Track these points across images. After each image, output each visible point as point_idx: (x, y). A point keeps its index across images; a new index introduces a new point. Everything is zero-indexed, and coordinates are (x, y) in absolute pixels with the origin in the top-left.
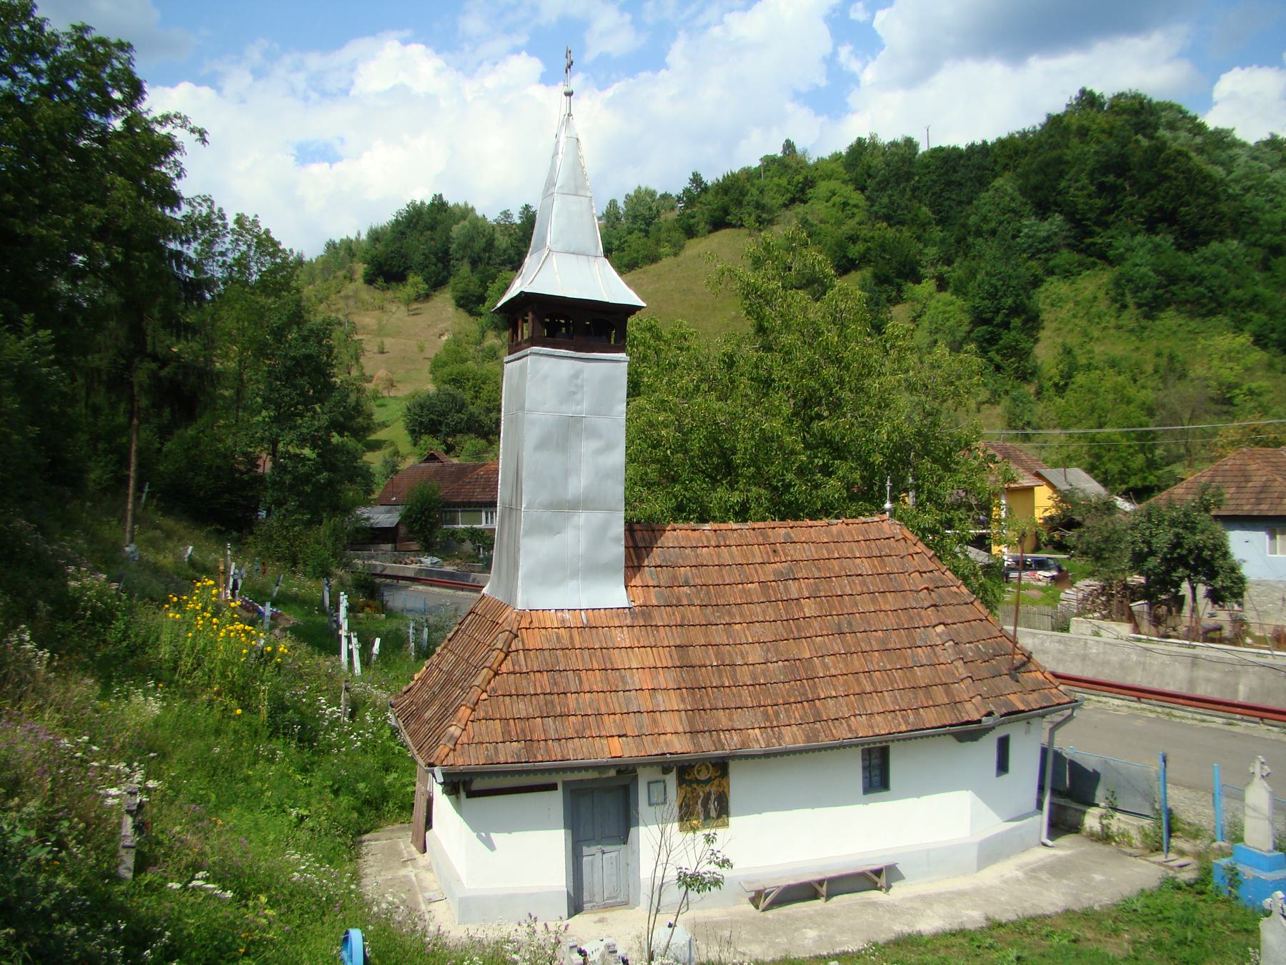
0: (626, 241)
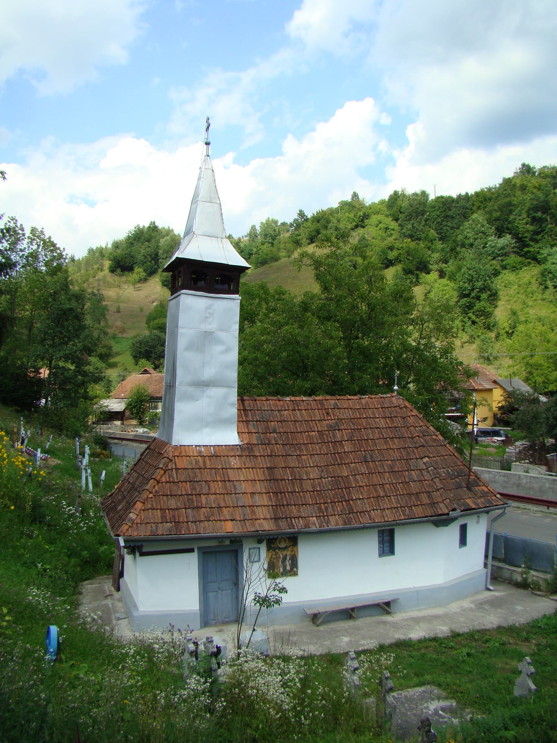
0: (260, 249)
